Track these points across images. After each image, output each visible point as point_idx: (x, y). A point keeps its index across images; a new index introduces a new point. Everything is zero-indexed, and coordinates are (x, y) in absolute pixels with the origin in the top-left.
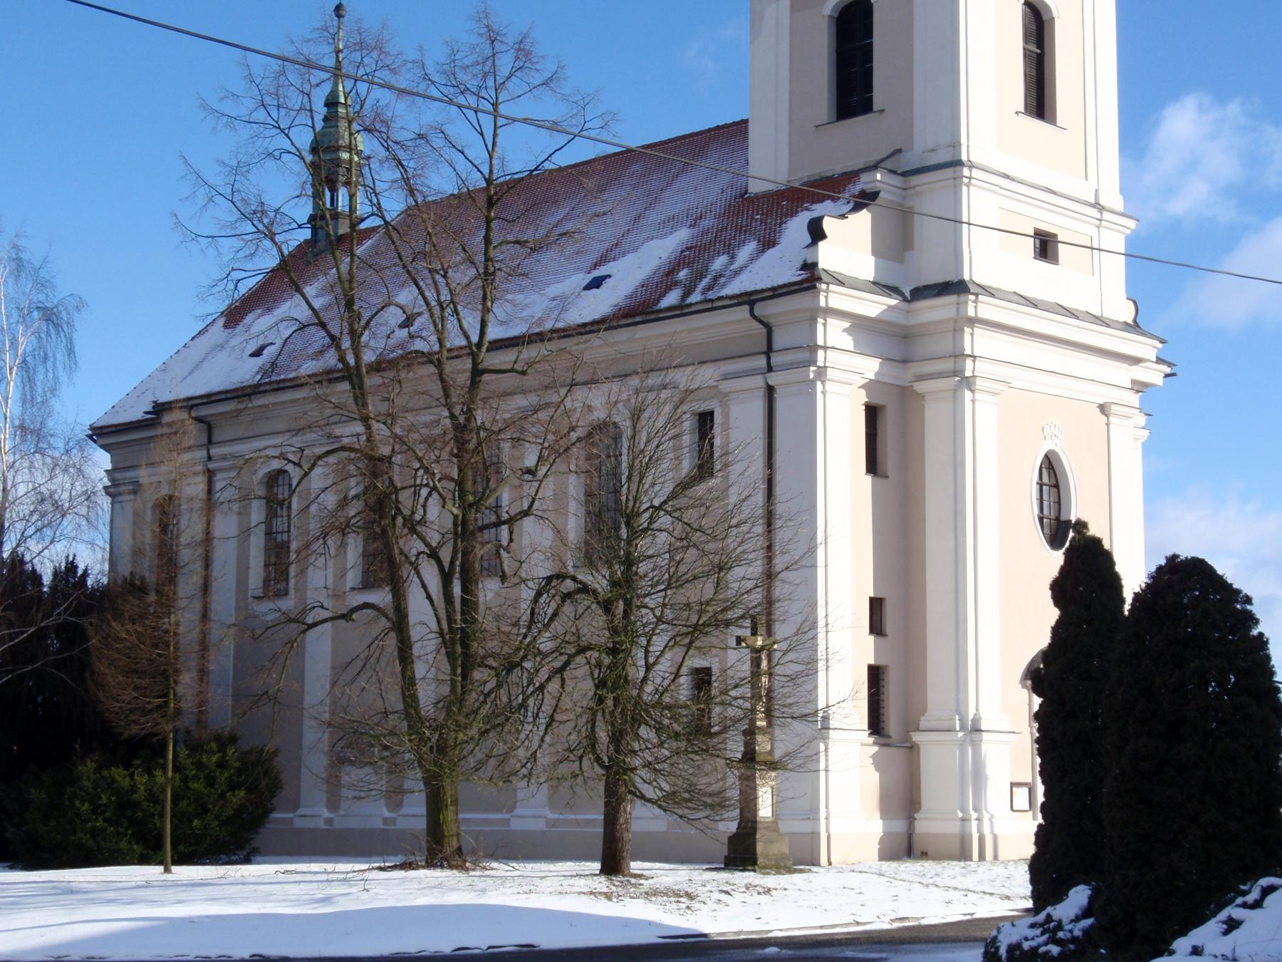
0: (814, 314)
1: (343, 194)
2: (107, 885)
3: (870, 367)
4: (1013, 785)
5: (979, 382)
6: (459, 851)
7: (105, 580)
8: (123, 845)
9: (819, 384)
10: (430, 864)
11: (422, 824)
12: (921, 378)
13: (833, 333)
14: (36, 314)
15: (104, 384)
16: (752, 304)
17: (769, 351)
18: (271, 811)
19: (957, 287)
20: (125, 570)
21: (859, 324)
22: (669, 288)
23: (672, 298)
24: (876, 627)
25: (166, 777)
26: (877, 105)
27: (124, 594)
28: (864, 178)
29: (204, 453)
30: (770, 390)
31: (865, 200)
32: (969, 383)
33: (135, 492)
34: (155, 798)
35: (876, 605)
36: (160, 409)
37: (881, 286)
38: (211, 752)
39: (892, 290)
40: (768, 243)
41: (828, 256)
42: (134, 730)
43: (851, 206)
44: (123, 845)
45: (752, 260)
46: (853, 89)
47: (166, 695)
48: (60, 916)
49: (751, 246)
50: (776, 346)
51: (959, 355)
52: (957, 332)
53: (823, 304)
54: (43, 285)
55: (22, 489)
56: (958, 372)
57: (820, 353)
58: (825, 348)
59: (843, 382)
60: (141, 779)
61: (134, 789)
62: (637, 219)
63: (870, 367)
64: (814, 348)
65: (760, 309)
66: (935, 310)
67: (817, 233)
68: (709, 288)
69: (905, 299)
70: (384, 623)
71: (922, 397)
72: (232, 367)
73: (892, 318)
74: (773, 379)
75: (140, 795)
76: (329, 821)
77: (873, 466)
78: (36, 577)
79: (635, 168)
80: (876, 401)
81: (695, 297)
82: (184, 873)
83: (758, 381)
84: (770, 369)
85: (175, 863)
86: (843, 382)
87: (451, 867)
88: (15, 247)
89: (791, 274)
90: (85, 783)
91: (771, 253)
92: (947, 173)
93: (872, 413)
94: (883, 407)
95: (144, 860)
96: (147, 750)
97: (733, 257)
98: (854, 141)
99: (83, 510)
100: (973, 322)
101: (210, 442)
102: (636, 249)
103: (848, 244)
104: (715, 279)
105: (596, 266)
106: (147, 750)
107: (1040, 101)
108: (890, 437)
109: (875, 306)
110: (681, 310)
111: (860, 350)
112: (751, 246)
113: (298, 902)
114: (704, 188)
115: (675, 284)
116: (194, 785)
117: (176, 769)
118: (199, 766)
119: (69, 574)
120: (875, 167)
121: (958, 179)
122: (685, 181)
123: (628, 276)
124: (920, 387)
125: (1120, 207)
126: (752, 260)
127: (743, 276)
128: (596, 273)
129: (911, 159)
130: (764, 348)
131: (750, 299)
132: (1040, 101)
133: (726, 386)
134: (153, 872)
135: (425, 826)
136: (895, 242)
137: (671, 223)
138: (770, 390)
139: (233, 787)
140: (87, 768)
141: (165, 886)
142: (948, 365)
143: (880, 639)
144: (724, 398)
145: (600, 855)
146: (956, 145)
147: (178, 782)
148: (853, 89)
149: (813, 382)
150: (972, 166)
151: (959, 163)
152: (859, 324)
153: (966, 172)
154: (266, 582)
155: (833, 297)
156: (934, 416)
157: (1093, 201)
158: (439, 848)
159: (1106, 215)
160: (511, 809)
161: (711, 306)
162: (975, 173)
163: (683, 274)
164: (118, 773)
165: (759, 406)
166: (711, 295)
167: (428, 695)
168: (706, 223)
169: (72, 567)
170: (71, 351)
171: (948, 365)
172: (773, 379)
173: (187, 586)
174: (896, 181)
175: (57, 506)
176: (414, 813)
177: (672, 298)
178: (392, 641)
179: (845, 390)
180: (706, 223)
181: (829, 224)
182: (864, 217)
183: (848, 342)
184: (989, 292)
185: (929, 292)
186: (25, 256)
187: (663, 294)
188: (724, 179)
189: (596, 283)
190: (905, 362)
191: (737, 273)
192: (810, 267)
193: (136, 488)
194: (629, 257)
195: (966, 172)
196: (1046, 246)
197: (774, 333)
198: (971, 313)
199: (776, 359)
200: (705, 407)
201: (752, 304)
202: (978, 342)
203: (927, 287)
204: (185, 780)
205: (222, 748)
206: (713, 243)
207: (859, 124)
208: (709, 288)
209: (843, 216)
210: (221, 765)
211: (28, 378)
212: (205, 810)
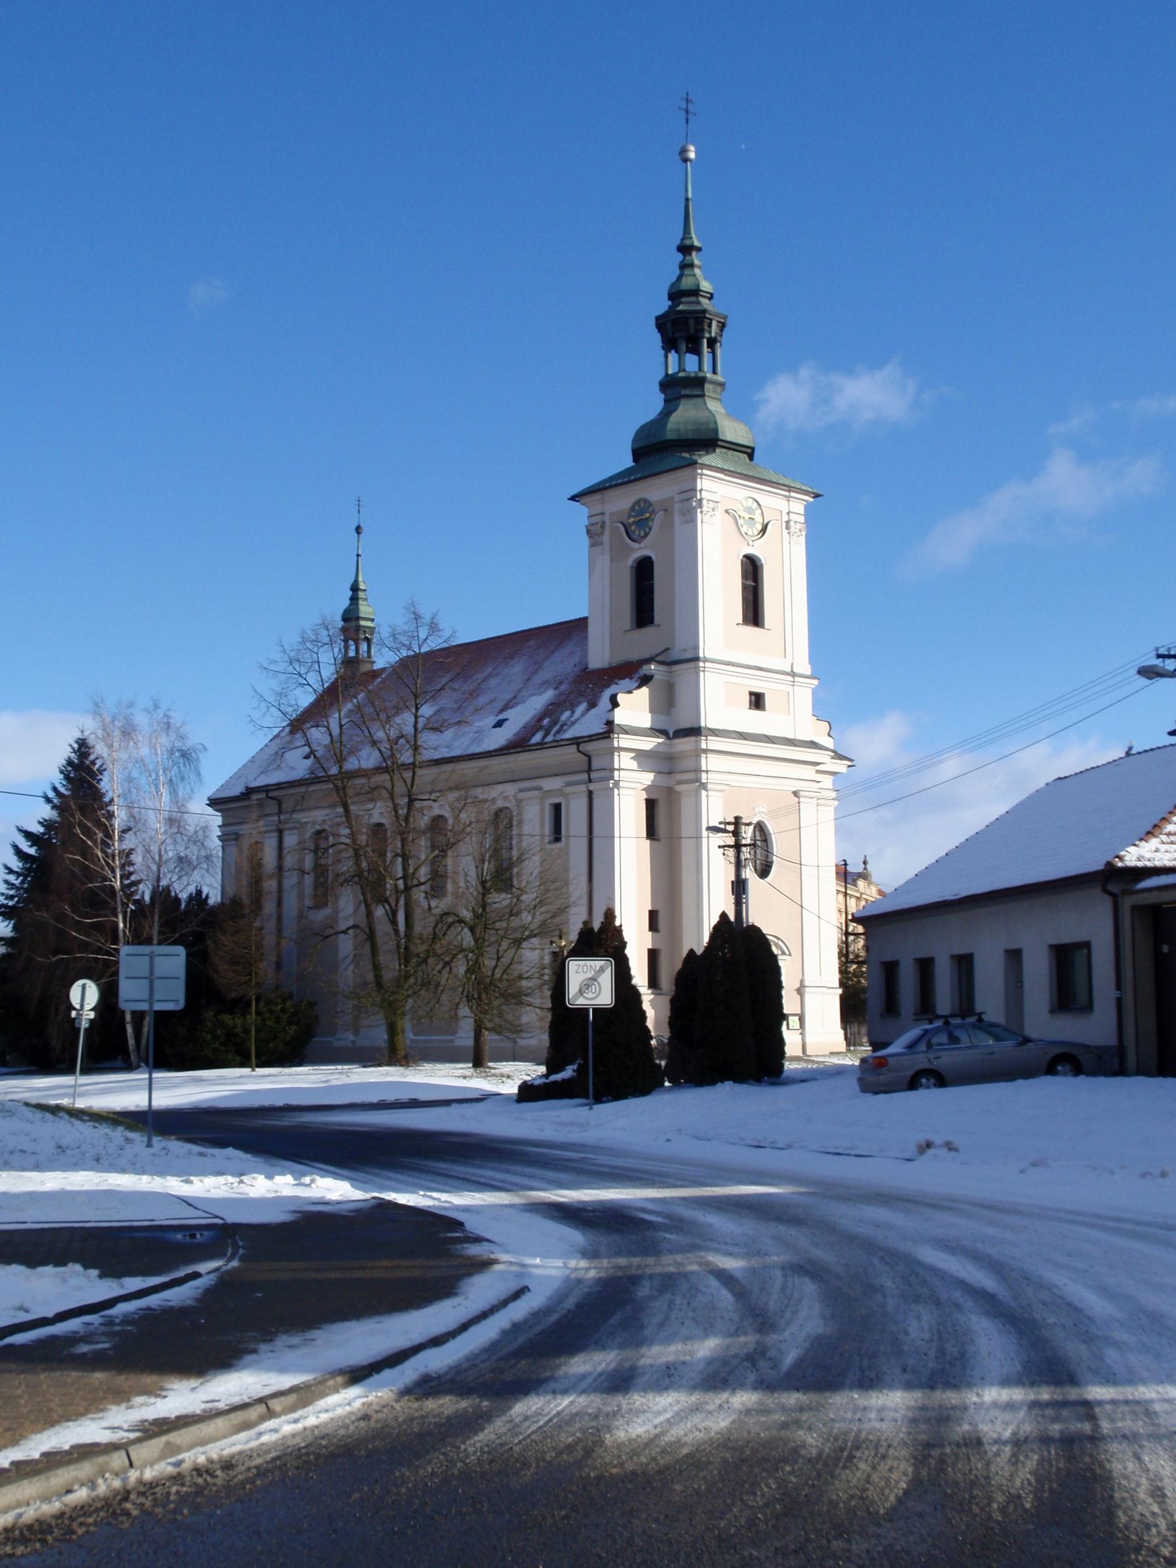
0: (612, 751)
1: (364, 647)
2: (221, 1078)
3: (648, 778)
5: (709, 786)
6: (405, 1057)
7: (219, 900)
8: (230, 1057)
9: (616, 791)
10: (389, 1064)
11: (471, 1042)
12: (679, 783)
13: (624, 761)
14: (177, 754)
15: (221, 770)
16: (578, 744)
17: (589, 770)
18: (313, 1037)
19: (695, 731)
20: (230, 891)
21: (640, 755)
22: (537, 731)
23: (537, 738)
24: (653, 926)
25: (252, 1017)
26: (657, 618)
27: (232, 908)
28: (645, 667)
29: (276, 818)
30: (590, 793)
31: (645, 681)
32: (704, 786)
33: (236, 839)
34: (247, 1032)
35: (653, 915)
36: (249, 792)
37: (656, 731)
38: (277, 1004)
39: (663, 732)
40: (592, 705)
41: (620, 717)
42: (233, 995)
43: (636, 684)
44: (230, 1057)
45: (583, 715)
46: (644, 610)
47: (250, 975)
48: (197, 1090)
49: (583, 706)
50: (593, 767)
51: (698, 770)
52: (698, 757)
53: (616, 745)
54: (182, 737)
55: (171, 854)
56: (698, 780)
57: (616, 773)
58: (619, 770)
59: (631, 788)
60: (239, 1021)
61: (235, 1026)
62: (529, 679)
63: (648, 778)
64: (612, 770)
65: (583, 747)
66: (684, 745)
67: (615, 704)
68: (558, 732)
69: (668, 738)
70: (363, 936)
71: (679, 793)
72: (297, 765)
73: (661, 749)
74: (592, 787)
75: (239, 1030)
76: (353, 1042)
77: (651, 833)
78: (177, 900)
79: (532, 643)
80: (652, 797)
81: (549, 738)
82: (261, 1071)
83: (583, 788)
84: (590, 781)
85: (259, 1066)
86: (631, 788)
87: (401, 1065)
88: (166, 716)
89: (600, 728)
90: (209, 1024)
91: (593, 711)
92: (691, 665)
93: (651, 805)
95: (242, 1065)
96: (240, 1005)
97: (573, 713)
98: (643, 643)
99: (205, 866)
100: (706, 751)
101: (280, 812)
102: (524, 702)
103: (634, 708)
104: (562, 726)
105: (502, 711)
106: (240, 1005)
107: (753, 613)
108: (660, 818)
109: (649, 744)
110: (541, 746)
111: (643, 768)
112: (583, 706)
113: (314, 1083)
114: (561, 664)
115: (541, 728)
116: (269, 1023)
117: (258, 1013)
118: (271, 1012)
119: (198, 898)
120: (648, 661)
121: (697, 671)
122: (558, 655)
123: (518, 718)
124: (678, 788)
125: (807, 670)
126: (583, 715)
127: (577, 726)
128: (501, 717)
129: (674, 655)
130: (586, 768)
131: (577, 741)
132: (753, 613)
133: (568, 790)
134: (246, 1071)
135: (547, 1044)
136: (665, 703)
137: (545, 684)
138: (590, 793)
139: (290, 1023)
140: (209, 1015)
141: (250, 1077)
142: (692, 776)
143: (656, 934)
144: (566, 796)
145: (472, 1057)
146: (696, 648)
147: (259, 1021)
148: (644, 610)
149: (612, 789)
150: (705, 660)
151: (697, 659)
152: (640, 755)
153: (701, 664)
154: (315, 896)
155: (622, 741)
156: (686, 804)
157: (789, 670)
158: (394, 1055)
159: (797, 679)
160: (454, 1034)
161: (557, 744)
162: (707, 664)
163: (546, 722)
164: (226, 1018)
165: (584, 801)
166: (558, 737)
167: (388, 976)
168: (563, 687)
169: (199, 892)
170: (199, 774)
171: (692, 776)
172: (592, 787)
173: (269, 906)
174: (663, 668)
175: (190, 863)
176: (379, 1036)
177: (537, 738)
178: (367, 946)
179: (633, 792)
180: (563, 687)
181: (621, 698)
182: (645, 691)
183: (634, 765)
184: (715, 732)
185: (680, 732)
186: (172, 721)
187: (533, 735)
188: (576, 659)
189: (499, 724)
190: (670, 773)
191: (573, 723)
192: (610, 723)
193: (237, 837)
194: (520, 706)
195: (701, 664)
196: (757, 701)
197: (591, 762)
198: (703, 746)
199: (593, 775)
200: (556, 800)
201: (578, 744)
202: (709, 762)
203: (682, 730)
204: (263, 1020)
205: (284, 1001)
206: (564, 702)
207: (647, 631)
208: (558, 732)
209: (630, 692)
210: (283, 1010)
211: (174, 792)
212: (275, 1038)
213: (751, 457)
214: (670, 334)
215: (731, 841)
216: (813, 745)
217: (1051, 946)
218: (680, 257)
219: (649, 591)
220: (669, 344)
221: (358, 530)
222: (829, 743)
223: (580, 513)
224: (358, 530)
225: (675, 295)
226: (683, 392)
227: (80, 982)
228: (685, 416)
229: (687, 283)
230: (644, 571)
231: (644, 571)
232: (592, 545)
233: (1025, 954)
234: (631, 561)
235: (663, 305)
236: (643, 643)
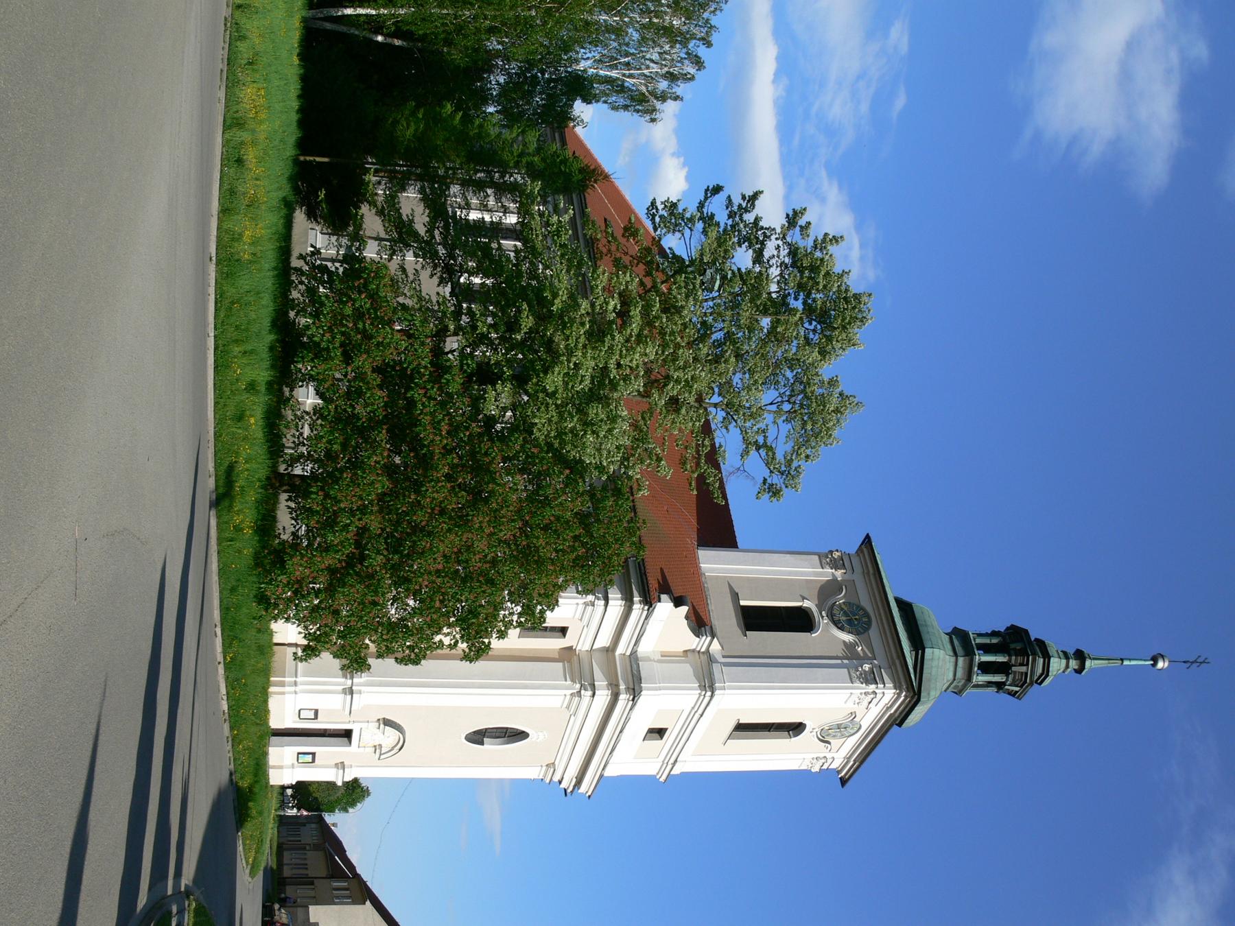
4: (316, 712)
46: (757, 619)
94: (564, 635)
98: (723, 615)
148: (757, 619)
214: (1012, 646)
226: (961, 660)
230: (798, 621)
231: (798, 621)
236: (723, 615)
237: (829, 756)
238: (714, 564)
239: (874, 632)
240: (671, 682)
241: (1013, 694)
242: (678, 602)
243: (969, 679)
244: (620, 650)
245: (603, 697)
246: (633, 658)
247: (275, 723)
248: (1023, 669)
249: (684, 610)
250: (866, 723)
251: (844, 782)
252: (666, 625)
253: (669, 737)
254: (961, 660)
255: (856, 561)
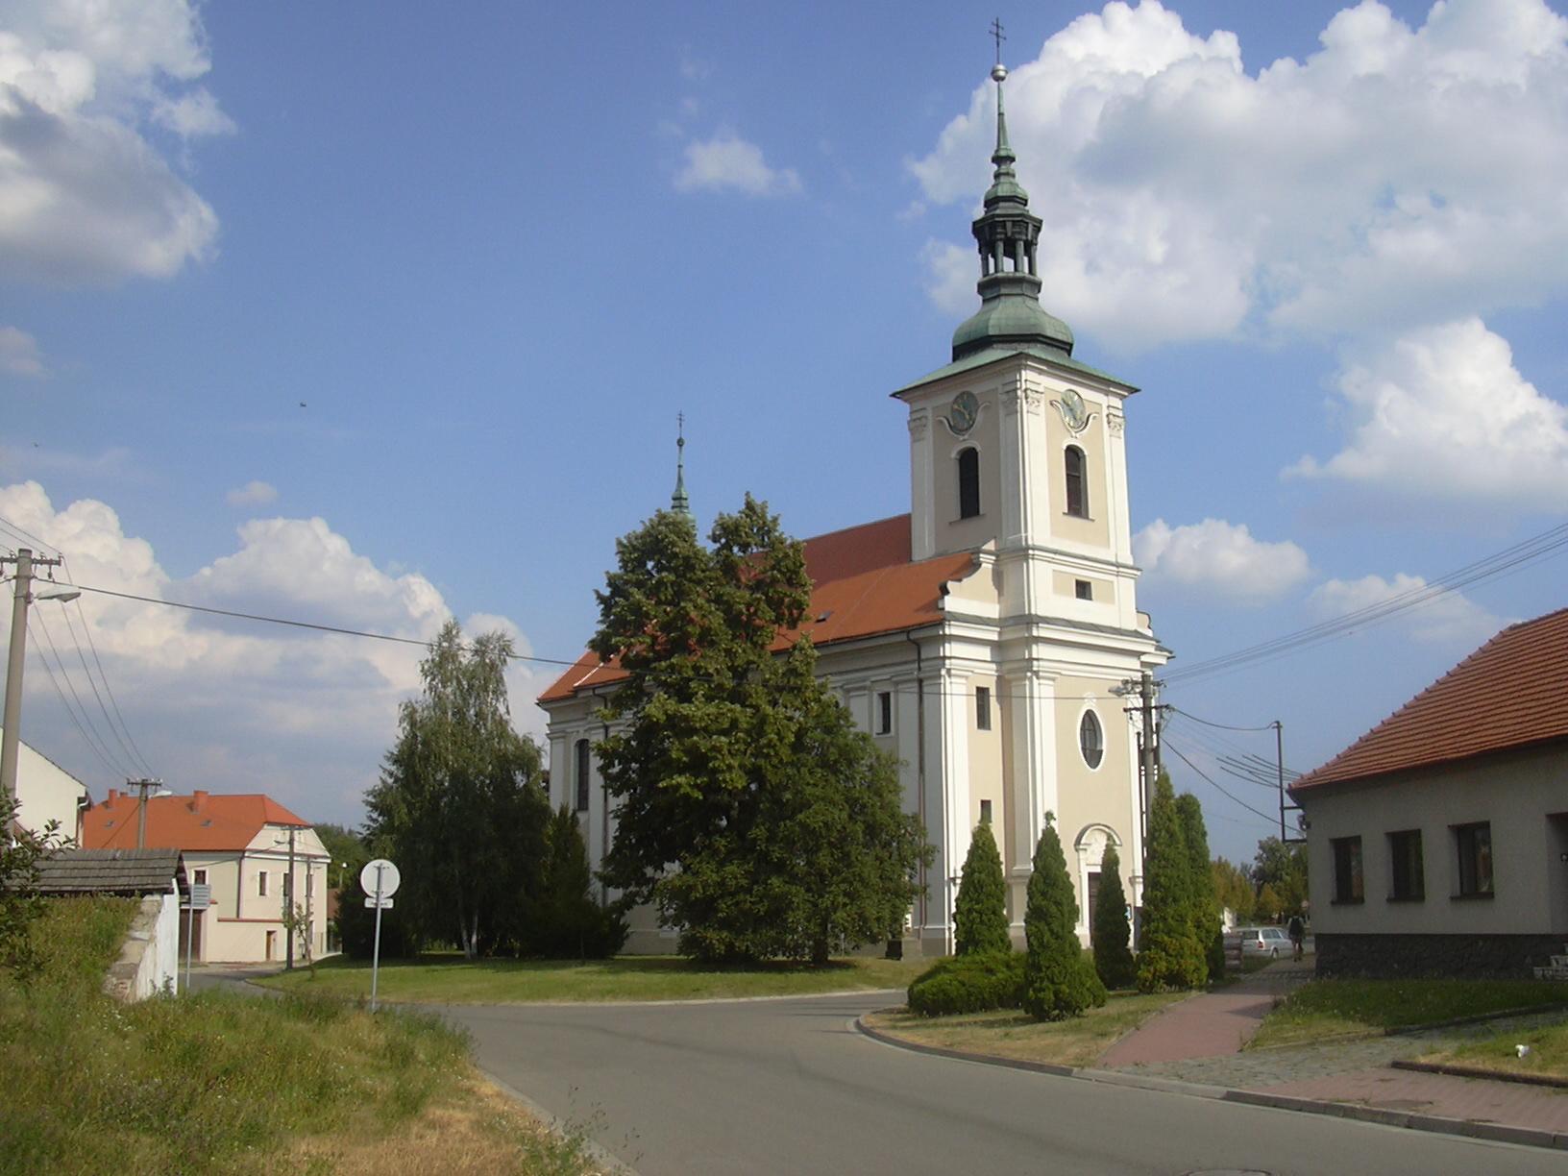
46: (970, 504)
107: (1077, 501)
132: (1077, 501)
148: (970, 504)
196: (1083, 589)
200: (886, 689)
213: (1069, 353)
215: (1139, 703)
216: (1136, 634)
217: (1388, 834)
218: (995, 167)
219: (975, 486)
220: (987, 248)
221: (680, 443)
222: (1150, 633)
223: (903, 408)
224: (680, 443)
225: (991, 202)
227: (376, 863)
228: (1006, 314)
229: (1003, 190)
230: (969, 462)
231: (969, 462)
232: (914, 441)
233: (1364, 842)
234: (954, 455)
235: (979, 212)
237: (1105, 412)
238: (924, 545)
239: (976, 390)
240: (1021, 592)
241: (1038, 229)
242: (945, 591)
243: (1020, 281)
244: (995, 637)
245: (1037, 651)
246: (1001, 623)
247: (263, 958)
248: (1009, 225)
249: (950, 585)
250: (1062, 386)
251: (1134, 390)
252: (970, 599)
253: (1085, 575)
254: (1003, 291)
255: (918, 406)
